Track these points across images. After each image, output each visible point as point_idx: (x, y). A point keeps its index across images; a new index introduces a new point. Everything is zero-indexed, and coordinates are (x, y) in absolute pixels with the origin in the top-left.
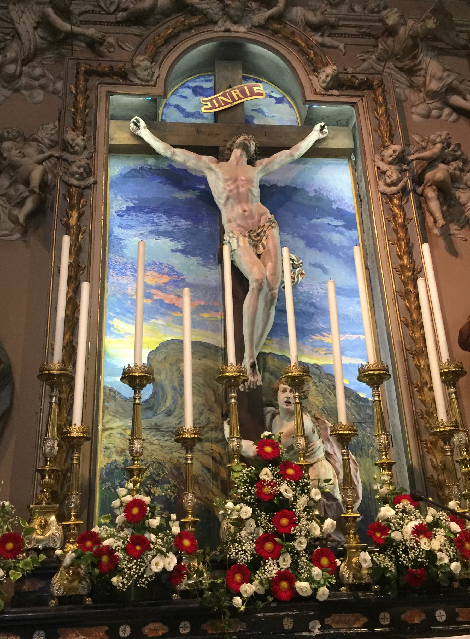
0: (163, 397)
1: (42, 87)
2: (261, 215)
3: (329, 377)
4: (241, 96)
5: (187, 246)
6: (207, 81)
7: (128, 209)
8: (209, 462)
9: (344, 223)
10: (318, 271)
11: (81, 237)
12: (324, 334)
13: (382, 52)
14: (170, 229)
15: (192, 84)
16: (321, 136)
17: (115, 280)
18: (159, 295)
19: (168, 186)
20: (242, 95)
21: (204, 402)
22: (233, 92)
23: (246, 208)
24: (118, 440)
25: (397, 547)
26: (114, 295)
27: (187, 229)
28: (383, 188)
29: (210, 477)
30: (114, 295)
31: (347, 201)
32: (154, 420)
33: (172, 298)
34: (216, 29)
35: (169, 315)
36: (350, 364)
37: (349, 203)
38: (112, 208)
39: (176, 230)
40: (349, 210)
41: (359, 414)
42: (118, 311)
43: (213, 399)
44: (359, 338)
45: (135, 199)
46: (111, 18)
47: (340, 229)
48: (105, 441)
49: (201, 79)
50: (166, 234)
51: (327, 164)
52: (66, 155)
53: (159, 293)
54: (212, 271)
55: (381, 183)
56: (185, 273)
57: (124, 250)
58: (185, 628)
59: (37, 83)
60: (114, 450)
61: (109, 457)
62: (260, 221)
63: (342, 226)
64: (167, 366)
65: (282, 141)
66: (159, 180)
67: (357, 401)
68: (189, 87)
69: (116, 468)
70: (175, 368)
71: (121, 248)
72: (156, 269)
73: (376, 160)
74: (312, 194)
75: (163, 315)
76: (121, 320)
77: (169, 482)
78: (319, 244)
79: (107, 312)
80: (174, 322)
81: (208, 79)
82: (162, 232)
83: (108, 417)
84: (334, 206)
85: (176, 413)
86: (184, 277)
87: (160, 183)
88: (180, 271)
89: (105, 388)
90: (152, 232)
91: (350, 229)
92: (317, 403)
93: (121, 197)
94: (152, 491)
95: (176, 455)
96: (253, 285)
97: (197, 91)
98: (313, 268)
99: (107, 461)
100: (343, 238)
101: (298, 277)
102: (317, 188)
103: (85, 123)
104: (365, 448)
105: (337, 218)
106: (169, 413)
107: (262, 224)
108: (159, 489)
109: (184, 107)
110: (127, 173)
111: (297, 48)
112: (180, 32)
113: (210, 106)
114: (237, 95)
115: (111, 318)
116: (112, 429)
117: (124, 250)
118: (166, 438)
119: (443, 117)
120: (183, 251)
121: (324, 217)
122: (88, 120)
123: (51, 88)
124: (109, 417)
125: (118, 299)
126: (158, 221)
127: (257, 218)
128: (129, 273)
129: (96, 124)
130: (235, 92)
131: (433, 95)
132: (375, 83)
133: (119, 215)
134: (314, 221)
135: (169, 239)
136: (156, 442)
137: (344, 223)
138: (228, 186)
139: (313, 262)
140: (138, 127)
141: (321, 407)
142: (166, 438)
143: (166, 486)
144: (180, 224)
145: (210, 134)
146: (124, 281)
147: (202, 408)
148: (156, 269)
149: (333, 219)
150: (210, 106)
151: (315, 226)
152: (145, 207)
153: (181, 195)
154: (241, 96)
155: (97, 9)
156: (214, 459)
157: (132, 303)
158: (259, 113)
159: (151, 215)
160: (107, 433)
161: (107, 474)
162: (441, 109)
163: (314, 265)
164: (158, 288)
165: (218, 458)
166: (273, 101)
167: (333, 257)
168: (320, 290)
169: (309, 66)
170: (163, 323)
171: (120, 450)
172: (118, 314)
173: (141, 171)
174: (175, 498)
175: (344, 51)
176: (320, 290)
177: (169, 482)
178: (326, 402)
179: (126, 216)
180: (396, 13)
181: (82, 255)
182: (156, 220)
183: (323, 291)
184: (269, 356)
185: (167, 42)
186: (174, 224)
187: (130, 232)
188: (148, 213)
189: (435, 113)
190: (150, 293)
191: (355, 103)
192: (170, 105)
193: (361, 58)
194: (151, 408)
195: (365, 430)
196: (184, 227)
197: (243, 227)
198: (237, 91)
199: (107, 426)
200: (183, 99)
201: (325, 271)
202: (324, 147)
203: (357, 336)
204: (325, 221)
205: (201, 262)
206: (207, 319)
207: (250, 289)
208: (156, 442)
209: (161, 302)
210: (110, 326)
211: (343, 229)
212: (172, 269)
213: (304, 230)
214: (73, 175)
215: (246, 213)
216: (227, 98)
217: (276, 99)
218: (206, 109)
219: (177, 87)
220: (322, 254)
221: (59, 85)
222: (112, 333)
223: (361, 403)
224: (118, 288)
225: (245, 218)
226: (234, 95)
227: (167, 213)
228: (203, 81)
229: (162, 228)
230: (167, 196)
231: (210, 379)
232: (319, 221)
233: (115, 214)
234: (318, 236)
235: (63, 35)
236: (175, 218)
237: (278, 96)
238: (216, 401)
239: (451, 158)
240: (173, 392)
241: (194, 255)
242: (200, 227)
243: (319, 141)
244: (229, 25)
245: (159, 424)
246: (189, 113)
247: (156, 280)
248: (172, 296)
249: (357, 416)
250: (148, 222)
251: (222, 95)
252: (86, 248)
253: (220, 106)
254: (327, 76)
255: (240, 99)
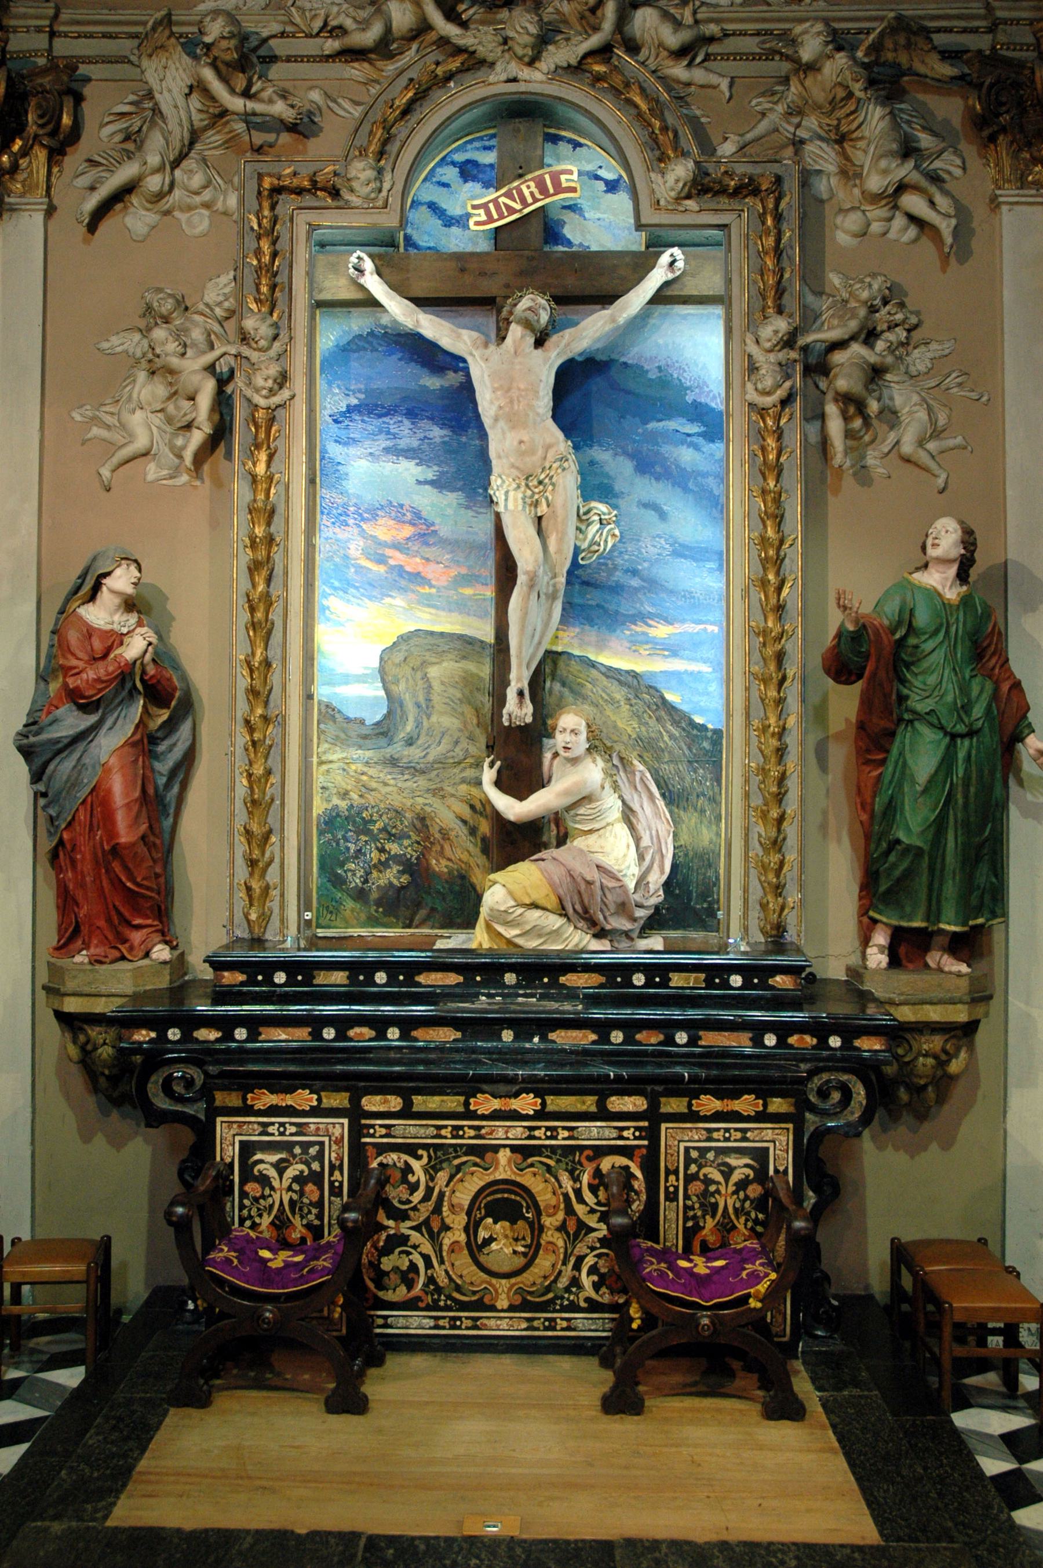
0: (401, 718)
1: (207, 205)
2: (548, 447)
3: (652, 691)
4: (538, 196)
5: (442, 473)
6: (486, 148)
7: (350, 409)
8: (466, 812)
9: (703, 429)
10: (651, 515)
11: (273, 491)
12: (651, 622)
13: (795, 98)
14: (415, 444)
15: (459, 157)
16: (670, 276)
17: (330, 534)
18: (397, 558)
19: (413, 364)
20: (541, 193)
21: (461, 726)
22: (524, 187)
23: (526, 438)
24: (339, 778)
25: (121, 1050)
26: (329, 559)
27: (444, 443)
28: (752, 396)
29: (466, 831)
30: (329, 559)
31: (712, 387)
32: (389, 751)
33: (417, 564)
34: (492, 78)
35: (413, 591)
36: (686, 671)
37: (716, 392)
38: (325, 408)
39: (425, 447)
40: (713, 405)
41: (690, 749)
42: (337, 584)
43: (475, 721)
44: (705, 630)
45: (360, 391)
46: (311, 47)
47: (694, 439)
48: (321, 779)
49: (477, 144)
50: (408, 453)
51: (684, 317)
52: (246, 351)
53: (398, 554)
54: (481, 516)
55: (749, 386)
56: (437, 521)
57: (344, 483)
58: (174, 1034)
59: (197, 199)
60: (335, 791)
61: (328, 801)
62: (545, 458)
63: (699, 434)
64: (407, 670)
65: (604, 284)
66: (400, 355)
67: (689, 729)
68: (454, 164)
69: (338, 815)
70: (419, 675)
71: (338, 478)
72: (393, 514)
73: (748, 341)
74: (652, 375)
75: (403, 590)
76: (341, 598)
77: (409, 837)
78: (658, 469)
79: (320, 587)
80: (419, 603)
81: (487, 143)
82: (402, 450)
83: (325, 746)
84: (689, 398)
85: (420, 742)
86: (437, 528)
87: (400, 359)
88: (431, 519)
89: (320, 703)
90: (387, 450)
91: (712, 440)
92: (629, 730)
93: (339, 387)
94: (387, 847)
95: (420, 800)
96: (522, 579)
97: (468, 171)
98: (643, 511)
99: (325, 805)
100: (698, 456)
101: (606, 541)
102: (662, 363)
103: (273, 287)
104: (693, 798)
105: (691, 420)
106: (410, 742)
107: (547, 465)
108: (396, 845)
109: (444, 206)
110: (348, 343)
111: (633, 111)
112: (429, 89)
113: (484, 218)
114: (532, 194)
115: (325, 596)
116: (331, 762)
117: (344, 483)
118: (406, 777)
119: (891, 235)
120: (436, 484)
121: (669, 417)
122: (278, 279)
123: (219, 206)
124: (326, 746)
125: (336, 565)
126: (396, 431)
127: (540, 453)
128: (351, 522)
129: (291, 289)
130: (528, 187)
131: (874, 198)
132: (764, 188)
133: (336, 421)
134: (652, 425)
135: (414, 462)
136: (392, 782)
137: (703, 429)
138: (497, 399)
139: (645, 500)
140: (361, 271)
141: (634, 736)
142: (406, 777)
143: (406, 842)
144: (431, 435)
145: (483, 274)
146: (342, 534)
147: (457, 734)
148: (393, 514)
149: (684, 421)
150: (484, 218)
151: (653, 437)
152: (377, 406)
153: (433, 382)
154: (538, 196)
155: (289, 29)
156: (472, 807)
157: (356, 572)
158: (574, 211)
159: (385, 419)
160: (324, 767)
161: (326, 823)
162: (890, 219)
163: (646, 505)
164: (396, 546)
165: (479, 806)
166: (601, 186)
167: (679, 490)
168: (651, 549)
169: (652, 150)
170: (403, 604)
171: (342, 791)
172: (335, 589)
173: (370, 339)
174: (418, 858)
175: (727, 95)
176: (651, 549)
177: (409, 837)
178: (643, 729)
179: (347, 423)
180: (819, 33)
181: (276, 518)
182: (394, 429)
183: (656, 551)
184: (564, 657)
185: (406, 111)
186: (422, 435)
187: (352, 451)
188: (380, 416)
189: (876, 227)
190: (383, 555)
191: (725, 226)
192: (421, 204)
193: (758, 108)
194: (384, 734)
195: (695, 772)
196: (438, 440)
197: (518, 468)
198: (532, 184)
199: (324, 758)
200: (442, 189)
201: (663, 516)
202: (676, 293)
203: (702, 627)
204: (672, 425)
205: (462, 501)
206: (470, 598)
207: (519, 582)
208: (392, 782)
209: (400, 570)
210: (324, 609)
211: (701, 441)
212: (417, 515)
213: (635, 441)
214: (257, 391)
215: (523, 447)
216: (514, 200)
217: (607, 182)
218: (477, 223)
219: (432, 165)
220: (661, 485)
221: (232, 201)
222: (328, 620)
223: (695, 732)
224: (335, 547)
225: (522, 454)
226: (526, 192)
227: (412, 414)
228: (478, 149)
229: (403, 443)
230: (412, 385)
231: (471, 692)
232: (661, 424)
233: (330, 420)
234: (657, 453)
235: (249, 1539)
236: (425, 424)
237: (610, 176)
238: (478, 725)
239: (885, 326)
240: (416, 710)
241: (453, 490)
242: (464, 439)
243: (667, 284)
244: (514, 69)
245: (396, 756)
246: (452, 218)
247: (394, 532)
248: (418, 560)
249: (687, 752)
250: (381, 432)
251: (505, 195)
252: (281, 509)
253: (501, 217)
254: (677, 181)
255: (536, 200)
